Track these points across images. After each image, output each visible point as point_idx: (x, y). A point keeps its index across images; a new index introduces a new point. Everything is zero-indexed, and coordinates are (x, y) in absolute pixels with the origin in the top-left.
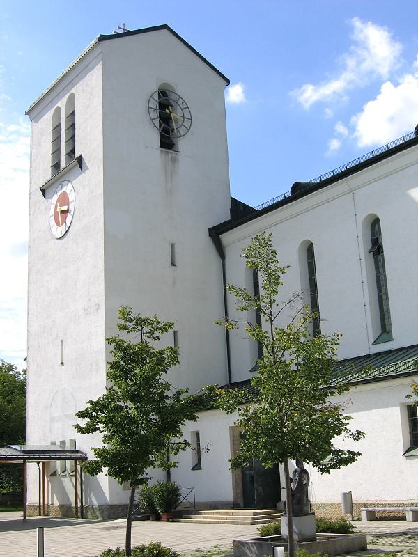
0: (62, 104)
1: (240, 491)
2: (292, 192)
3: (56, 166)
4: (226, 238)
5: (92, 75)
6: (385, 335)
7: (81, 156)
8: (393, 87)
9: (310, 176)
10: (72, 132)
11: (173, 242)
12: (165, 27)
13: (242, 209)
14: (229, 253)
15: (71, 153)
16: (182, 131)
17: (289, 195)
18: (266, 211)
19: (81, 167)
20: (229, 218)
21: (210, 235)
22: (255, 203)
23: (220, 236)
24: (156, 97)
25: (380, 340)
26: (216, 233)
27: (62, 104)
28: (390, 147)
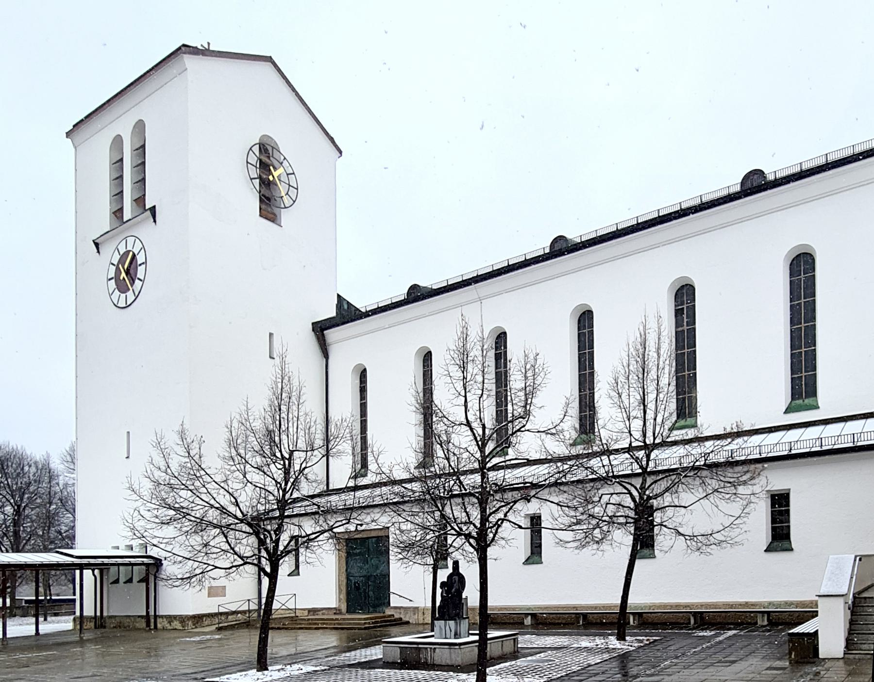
0: (124, 127)
1: (343, 596)
2: (409, 293)
3: (118, 213)
4: (331, 335)
5: (767, 542)
6: (536, 558)
7: (154, 207)
8: (130, 584)
9: (428, 281)
10: (143, 175)
11: (272, 332)
12: (269, 59)
13: (346, 307)
14: (334, 352)
15: (140, 201)
16: (287, 201)
17: (738, 188)
18: (367, 314)
19: (155, 221)
20: (334, 314)
21: (313, 330)
22: (362, 303)
23: (325, 332)
24: (256, 149)
25: (531, 561)
26: (320, 329)
27: (124, 127)
28: (704, 200)
